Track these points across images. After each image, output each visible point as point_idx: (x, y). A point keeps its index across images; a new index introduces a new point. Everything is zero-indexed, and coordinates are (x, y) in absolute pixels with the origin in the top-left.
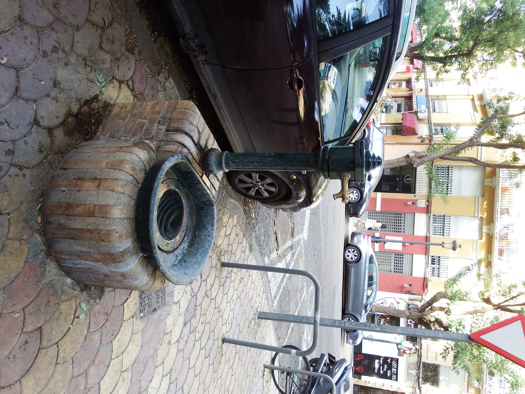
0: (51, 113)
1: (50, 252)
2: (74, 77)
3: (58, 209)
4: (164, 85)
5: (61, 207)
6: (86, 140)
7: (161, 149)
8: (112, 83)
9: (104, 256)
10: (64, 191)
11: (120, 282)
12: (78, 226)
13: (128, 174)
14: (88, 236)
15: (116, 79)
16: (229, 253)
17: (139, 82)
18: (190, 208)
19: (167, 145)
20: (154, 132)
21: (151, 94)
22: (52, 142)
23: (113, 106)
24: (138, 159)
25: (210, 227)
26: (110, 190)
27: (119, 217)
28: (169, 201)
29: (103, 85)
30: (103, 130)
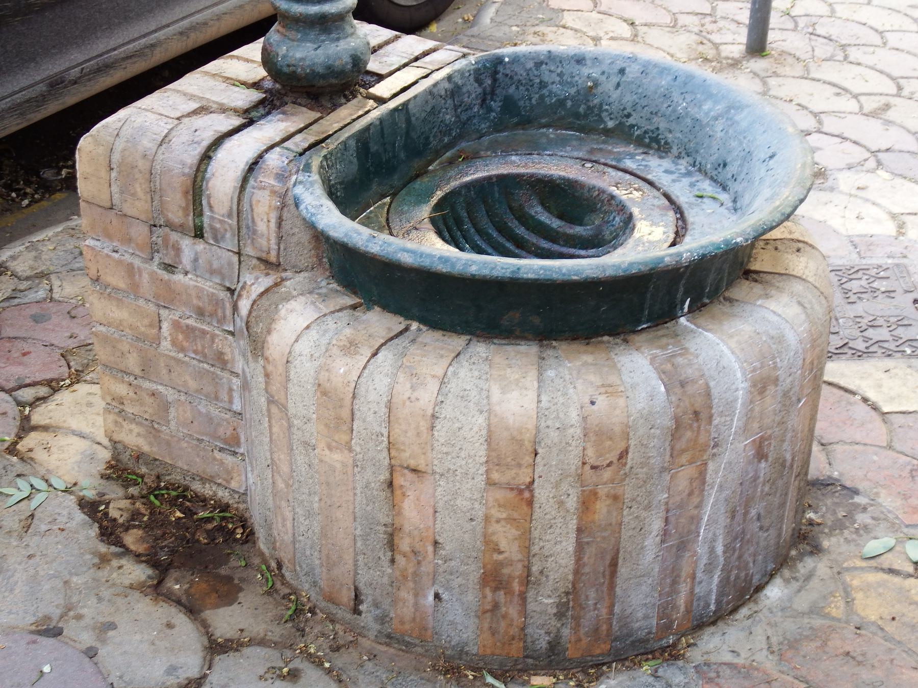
0: (153, 644)
1: (663, 650)
2: (17, 575)
3: (504, 617)
4: (27, 278)
5: (496, 606)
6: (250, 536)
7: (273, 253)
8: (31, 454)
9: (683, 451)
10: (437, 596)
11: (787, 400)
12: (569, 545)
13: (370, 367)
14: (604, 510)
15: (15, 443)
16: (710, 27)
17: (20, 364)
18: (508, 149)
19: (255, 232)
20: (209, 286)
21: (64, 323)
22: (262, 642)
23: (119, 446)
24: (313, 334)
25: (586, 71)
26: (432, 428)
27: (532, 395)
28: (480, 232)
29: (39, 484)
30: (211, 480)
